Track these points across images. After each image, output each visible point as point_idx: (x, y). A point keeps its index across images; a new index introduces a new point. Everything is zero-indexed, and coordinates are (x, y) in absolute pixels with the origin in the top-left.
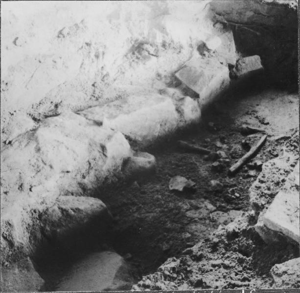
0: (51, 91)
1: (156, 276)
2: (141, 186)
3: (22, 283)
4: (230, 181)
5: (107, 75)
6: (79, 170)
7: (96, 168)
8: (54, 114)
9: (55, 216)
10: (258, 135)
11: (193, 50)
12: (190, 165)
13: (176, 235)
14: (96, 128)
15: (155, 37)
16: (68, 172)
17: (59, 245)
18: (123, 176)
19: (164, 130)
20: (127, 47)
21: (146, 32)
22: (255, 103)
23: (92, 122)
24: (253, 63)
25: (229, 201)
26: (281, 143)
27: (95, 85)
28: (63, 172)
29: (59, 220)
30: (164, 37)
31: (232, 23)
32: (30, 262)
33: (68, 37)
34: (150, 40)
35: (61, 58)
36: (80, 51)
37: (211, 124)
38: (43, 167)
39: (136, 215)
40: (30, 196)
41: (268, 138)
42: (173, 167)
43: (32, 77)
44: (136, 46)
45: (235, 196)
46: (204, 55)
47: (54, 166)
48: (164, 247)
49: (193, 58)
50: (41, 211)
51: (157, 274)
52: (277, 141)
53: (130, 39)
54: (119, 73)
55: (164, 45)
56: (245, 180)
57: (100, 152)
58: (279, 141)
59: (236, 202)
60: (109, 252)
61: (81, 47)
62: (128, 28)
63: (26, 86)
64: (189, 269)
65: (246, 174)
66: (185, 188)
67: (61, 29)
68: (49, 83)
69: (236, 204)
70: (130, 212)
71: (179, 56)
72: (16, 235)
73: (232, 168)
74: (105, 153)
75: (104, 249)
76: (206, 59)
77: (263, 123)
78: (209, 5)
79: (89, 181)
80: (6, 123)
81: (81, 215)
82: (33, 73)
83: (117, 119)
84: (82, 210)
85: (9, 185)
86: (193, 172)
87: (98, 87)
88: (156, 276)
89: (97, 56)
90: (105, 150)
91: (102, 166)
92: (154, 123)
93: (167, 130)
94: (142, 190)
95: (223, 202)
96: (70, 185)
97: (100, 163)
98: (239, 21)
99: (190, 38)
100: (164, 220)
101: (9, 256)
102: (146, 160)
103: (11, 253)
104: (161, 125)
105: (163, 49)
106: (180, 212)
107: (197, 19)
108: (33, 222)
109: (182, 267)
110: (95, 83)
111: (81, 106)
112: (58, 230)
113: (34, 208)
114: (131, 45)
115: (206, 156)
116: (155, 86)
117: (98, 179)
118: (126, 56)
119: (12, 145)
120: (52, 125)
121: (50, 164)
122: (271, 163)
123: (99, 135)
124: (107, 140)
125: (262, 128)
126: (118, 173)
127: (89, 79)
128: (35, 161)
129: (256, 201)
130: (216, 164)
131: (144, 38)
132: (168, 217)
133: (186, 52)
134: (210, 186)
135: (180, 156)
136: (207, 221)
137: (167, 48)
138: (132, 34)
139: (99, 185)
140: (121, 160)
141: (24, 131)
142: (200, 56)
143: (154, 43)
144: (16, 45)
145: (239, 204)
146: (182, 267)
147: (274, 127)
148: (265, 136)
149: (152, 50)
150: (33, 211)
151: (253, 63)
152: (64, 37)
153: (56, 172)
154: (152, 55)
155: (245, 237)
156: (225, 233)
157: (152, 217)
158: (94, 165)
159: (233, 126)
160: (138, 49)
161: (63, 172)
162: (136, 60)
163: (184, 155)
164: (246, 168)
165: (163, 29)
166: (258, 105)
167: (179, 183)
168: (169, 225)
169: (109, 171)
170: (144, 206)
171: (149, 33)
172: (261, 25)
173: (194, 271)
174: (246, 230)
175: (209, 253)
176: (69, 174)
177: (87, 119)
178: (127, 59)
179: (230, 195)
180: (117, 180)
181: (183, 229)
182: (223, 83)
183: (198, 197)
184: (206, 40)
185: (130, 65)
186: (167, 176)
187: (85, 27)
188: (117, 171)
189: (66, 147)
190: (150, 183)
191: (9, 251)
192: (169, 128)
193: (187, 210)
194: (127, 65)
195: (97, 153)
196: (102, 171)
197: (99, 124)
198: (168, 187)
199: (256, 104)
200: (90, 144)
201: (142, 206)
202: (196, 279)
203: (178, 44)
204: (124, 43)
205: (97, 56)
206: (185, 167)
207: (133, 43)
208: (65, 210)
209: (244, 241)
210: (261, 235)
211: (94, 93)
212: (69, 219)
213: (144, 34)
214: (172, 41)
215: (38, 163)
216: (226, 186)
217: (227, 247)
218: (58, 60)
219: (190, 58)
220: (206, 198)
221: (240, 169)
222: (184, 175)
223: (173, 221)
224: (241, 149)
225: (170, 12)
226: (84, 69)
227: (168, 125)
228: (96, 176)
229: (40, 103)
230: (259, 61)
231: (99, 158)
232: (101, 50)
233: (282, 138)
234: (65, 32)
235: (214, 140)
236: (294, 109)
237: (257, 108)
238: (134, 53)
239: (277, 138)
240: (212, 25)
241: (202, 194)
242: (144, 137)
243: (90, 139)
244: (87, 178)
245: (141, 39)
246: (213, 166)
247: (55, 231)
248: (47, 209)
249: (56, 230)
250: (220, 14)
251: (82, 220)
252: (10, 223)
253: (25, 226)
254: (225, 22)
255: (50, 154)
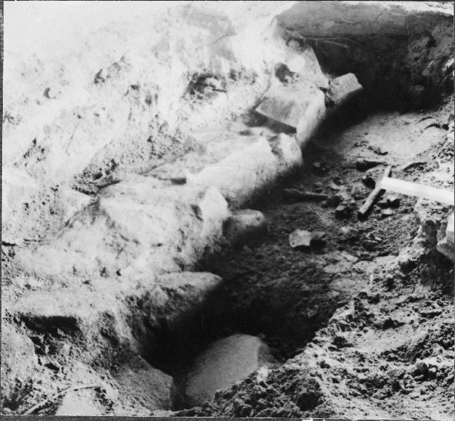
0: (96, 154)
1: (332, 328)
2: (253, 251)
3: (144, 384)
4: (365, 225)
5: (165, 124)
6: (171, 243)
7: (192, 236)
8: (110, 182)
9: (160, 300)
10: (380, 168)
11: (270, 77)
12: (308, 216)
13: (320, 297)
14: (178, 187)
15: (219, 67)
16: (159, 245)
17: (168, 340)
18: (227, 242)
19: (262, 180)
20: (183, 85)
21: (207, 62)
22: (361, 133)
23: (169, 182)
24: (348, 84)
25: (371, 248)
26: (411, 172)
27: (153, 140)
28: (153, 246)
29: (166, 304)
30: (231, 64)
31: (309, 38)
32: (143, 360)
33: (109, 80)
34: (214, 71)
35: (104, 109)
36: (126, 98)
37: (317, 165)
38: (125, 245)
39: (258, 285)
40: (120, 281)
41: (393, 170)
42: (287, 221)
43: (72, 138)
44: (195, 82)
45: (376, 240)
46: (286, 81)
47: (139, 240)
48: (309, 314)
49: (272, 87)
50: (140, 298)
51: (332, 326)
52: (405, 170)
53: (187, 74)
54: (180, 120)
55: (232, 76)
56: (382, 222)
57: (192, 215)
58: (408, 170)
59: (379, 246)
60: (238, 335)
61: (125, 92)
62: (182, 60)
63: (66, 151)
64: (368, 313)
65: (380, 215)
66: (312, 242)
67: (98, 71)
68: (93, 144)
69: (380, 249)
70: (250, 283)
71: (253, 87)
72: (119, 329)
73: (363, 209)
74: (199, 215)
75: (227, 335)
76: (290, 86)
77: (380, 154)
78: (276, 20)
79: (187, 255)
80: (52, 202)
81: (193, 293)
82: (72, 132)
83: (203, 172)
84: (193, 287)
85: (86, 273)
86: (314, 222)
87: (156, 142)
88: (332, 328)
89: (149, 102)
90: (199, 212)
91: (199, 233)
92: (249, 172)
93: (265, 178)
94: (257, 254)
95: (363, 251)
96: (165, 262)
97: (195, 230)
98: (318, 35)
99: (265, 62)
100: (298, 283)
101: (114, 358)
102: (250, 218)
103: (115, 353)
104: (257, 173)
105: (232, 81)
106: (316, 269)
107: (266, 39)
108: (133, 312)
109: (359, 313)
110: (150, 137)
111: (141, 168)
112: (168, 317)
113: (129, 295)
114: (188, 82)
115: (324, 202)
116: (232, 129)
117: (196, 251)
118: (183, 97)
119: (71, 226)
120: (117, 194)
121: (133, 238)
122: (429, 177)
123: (186, 194)
124: (199, 199)
125: (381, 159)
126: (220, 239)
127: (141, 133)
128: (112, 238)
129: (428, 219)
130: (340, 208)
131: (205, 70)
132: (302, 279)
133: (261, 80)
134: (341, 234)
135: (290, 207)
136: (354, 274)
137: (238, 79)
138: (188, 67)
139: (199, 258)
140: (220, 221)
141: (80, 208)
142: (281, 84)
143: (219, 75)
144: (48, 97)
145: (385, 248)
146: (359, 313)
147: (395, 156)
148: (389, 168)
149: (218, 84)
150: (128, 299)
151: (348, 84)
152: (103, 81)
153: (147, 248)
154: (218, 90)
155: (425, 263)
156: (398, 266)
157: (282, 283)
158: (188, 233)
159: (344, 162)
160: (198, 84)
161: (153, 246)
162: (199, 101)
163: (297, 205)
164: (378, 208)
165: (228, 55)
166: (366, 134)
167: (302, 237)
168: (306, 288)
169: (208, 238)
170: (257, 284)
171: (211, 63)
172: (347, 35)
173: (376, 313)
174: (424, 255)
175: (385, 292)
176: (161, 248)
177: (160, 179)
178: (185, 101)
179: (370, 241)
180: (220, 248)
181: (326, 289)
182: (319, 111)
183: (331, 250)
184: (286, 61)
185: (193, 108)
186: (283, 232)
187: (129, 65)
188: (219, 237)
189: (148, 215)
190: (264, 245)
191: (113, 351)
192: (268, 176)
193: (324, 266)
194: (187, 109)
195: (188, 217)
196: (200, 238)
197: (181, 182)
198: (289, 245)
199: (364, 132)
200: (177, 208)
201: (264, 274)
202: (383, 320)
203: (251, 71)
204: (179, 80)
205: (149, 102)
206: (301, 219)
207: (191, 78)
208: (172, 290)
209: (424, 267)
210: (446, 254)
211: (153, 150)
212: (179, 301)
213: (204, 64)
214: (243, 69)
215: (117, 241)
216: (361, 232)
217: (407, 282)
218: (101, 112)
219: (269, 87)
220: (341, 250)
221: (371, 209)
222: (304, 228)
223: (309, 283)
224: (364, 187)
225: (236, 31)
226: (134, 120)
227: (266, 171)
228: (193, 247)
229: (85, 173)
230: (355, 80)
231: (193, 223)
232: (153, 93)
233: (411, 166)
234: (104, 75)
235: (326, 182)
236: (413, 131)
237: (366, 138)
238: (192, 93)
239: (404, 167)
240: (284, 44)
241: (335, 246)
242: (238, 192)
243: (176, 201)
244: (183, 250)
245: (200, 72)
246: (337, 211)
247: (165, 319)
248: (148, 293)
249: (165, 318)
250: (292, 29)
251: (196, 299)
252: (110, 313)
253: (124, 318)
254: (300, 36)
255: (128, 225)
